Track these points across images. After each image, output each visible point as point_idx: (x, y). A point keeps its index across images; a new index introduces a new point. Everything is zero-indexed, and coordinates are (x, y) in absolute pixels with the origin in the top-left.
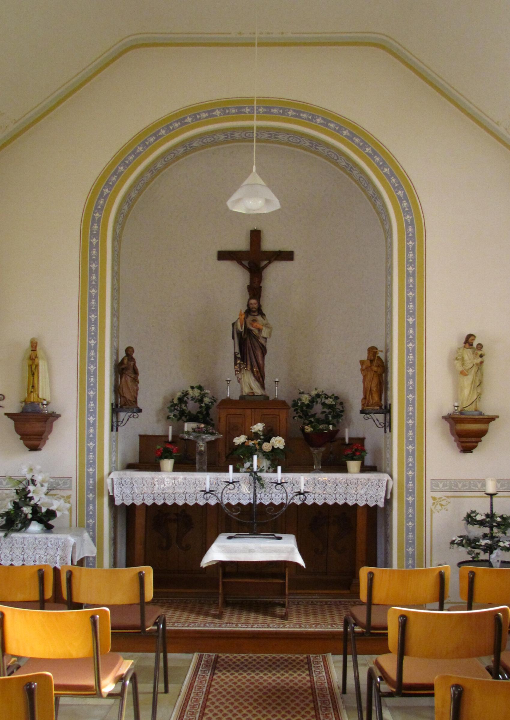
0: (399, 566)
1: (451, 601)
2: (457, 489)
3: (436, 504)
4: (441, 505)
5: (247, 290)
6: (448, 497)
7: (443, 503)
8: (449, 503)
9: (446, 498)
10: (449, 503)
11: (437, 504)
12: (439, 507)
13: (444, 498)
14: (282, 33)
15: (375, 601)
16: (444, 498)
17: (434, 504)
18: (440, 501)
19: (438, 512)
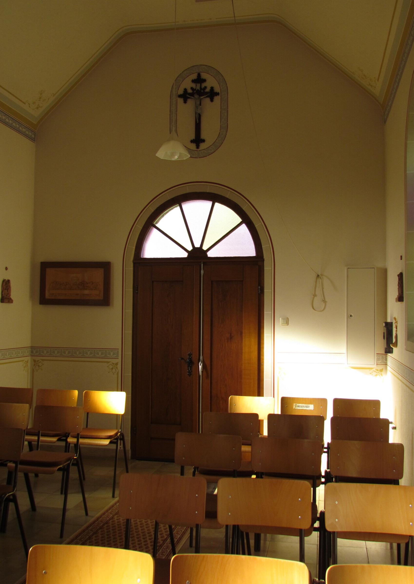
0: (41, 440)
1: (369, 370)
2: (65, 355)
3: (113, 365)
4: (112, 369)
5: (109, 261)
6: (118, 373)
7: (114, 370)
8: (114, 374)
9: (117, 372)
10: (114, 374)
11: (113, 366)
12: (111, 367)
13: (40, 361)
14: (211, 19)
15: (235, 16)
16: (40, 361)
17: (113, 364)
18: (115, 368)
19: (108, 367)
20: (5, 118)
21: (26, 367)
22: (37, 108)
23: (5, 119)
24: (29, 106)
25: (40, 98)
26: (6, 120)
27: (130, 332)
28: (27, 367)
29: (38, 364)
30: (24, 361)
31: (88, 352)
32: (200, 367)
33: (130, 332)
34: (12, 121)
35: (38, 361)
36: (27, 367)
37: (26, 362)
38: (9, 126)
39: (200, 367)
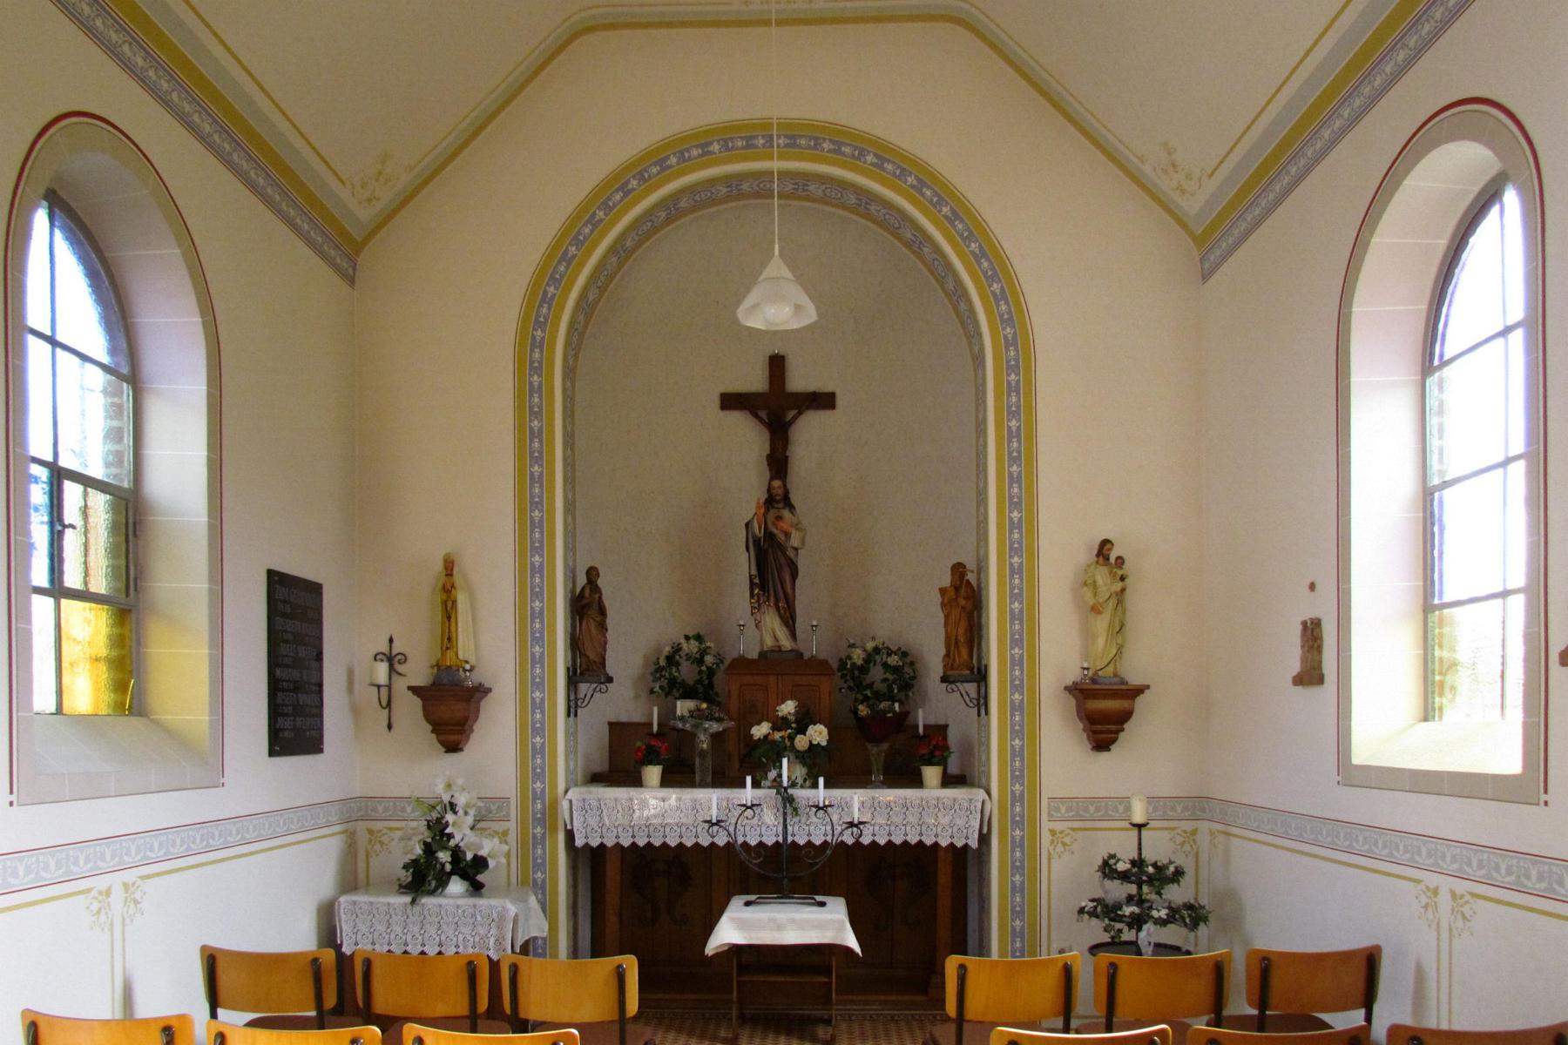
7: (1067, 840)
11: (1057, 843)
17: (1052, 841)
20: (120, 42)
21: (103, 912)
22: (369, 200)
23: (117, 42)
24: (353, 195)
25: (380, 173)
26: (192, 116)
27: (204, 651)
28: (107, 913)
29: (132, 896)
30: (94, 893)
31: (407, 805)
32: (132, 682)
33: (204, 651)
34: (211, 126)
35: (1062, 832)
36: (107, 913)
37: (100, 893)
38: (69, 15)
39: (132, 682)
